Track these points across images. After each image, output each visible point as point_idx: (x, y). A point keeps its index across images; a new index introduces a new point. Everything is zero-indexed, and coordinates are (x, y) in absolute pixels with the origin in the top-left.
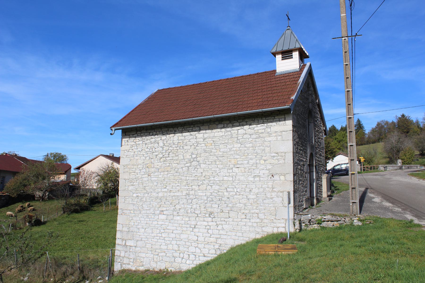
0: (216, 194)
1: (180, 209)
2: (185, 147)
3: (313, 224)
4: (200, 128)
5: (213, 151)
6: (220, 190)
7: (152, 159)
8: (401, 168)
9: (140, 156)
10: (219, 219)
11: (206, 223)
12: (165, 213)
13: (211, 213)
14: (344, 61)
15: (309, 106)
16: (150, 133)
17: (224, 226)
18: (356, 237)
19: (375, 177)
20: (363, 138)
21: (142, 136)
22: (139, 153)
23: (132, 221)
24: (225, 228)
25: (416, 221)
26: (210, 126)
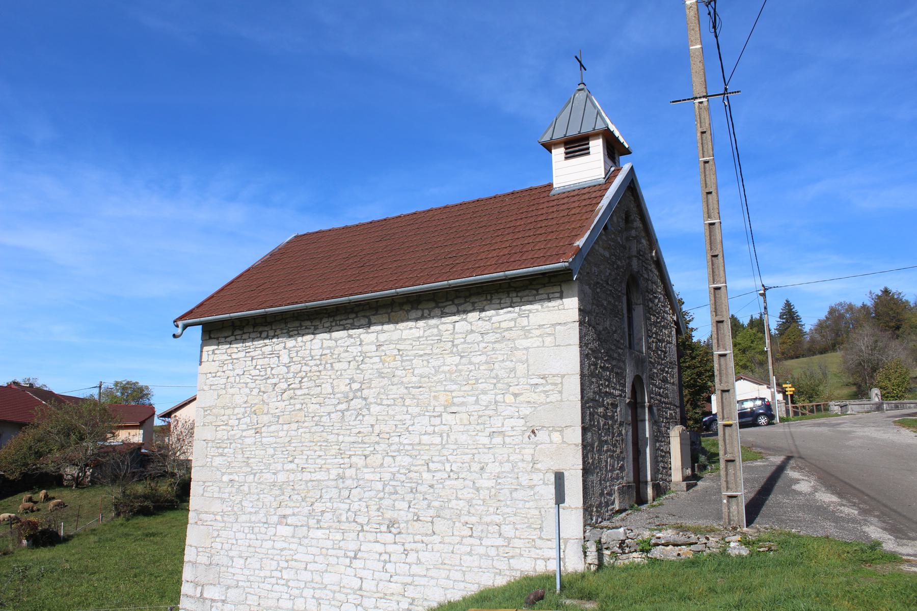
0: (403, 478)
1: (323, 512)
2: (337, 366)
3: (630, 552)
4: (370, 320)
5: (398, 373)
6: (412, 468)
7: (264, 392)
8: (879, 407)
9: (239, 386)
10: (410, 538)
11: (379, 548)
12: (289, 521)
13: (392, 524)
14: (701, 154)
15: (629, 265)
16: (261, 333)
17: (421, 554)
18: (724, 592)
19: (815, 429)
20: (800, 342)
21: (244, 341)
22: (238, 379)
23: (218, 540)
24: (423, 560)
25: (890, 544)
26: (393, 314)
